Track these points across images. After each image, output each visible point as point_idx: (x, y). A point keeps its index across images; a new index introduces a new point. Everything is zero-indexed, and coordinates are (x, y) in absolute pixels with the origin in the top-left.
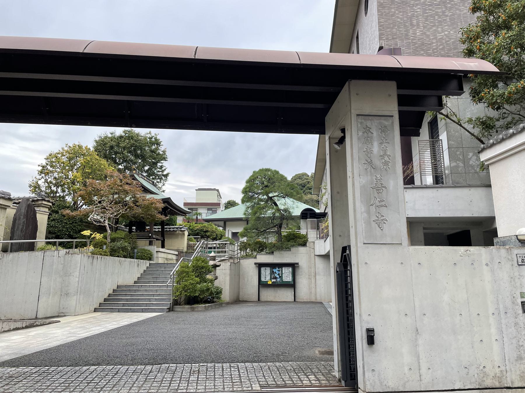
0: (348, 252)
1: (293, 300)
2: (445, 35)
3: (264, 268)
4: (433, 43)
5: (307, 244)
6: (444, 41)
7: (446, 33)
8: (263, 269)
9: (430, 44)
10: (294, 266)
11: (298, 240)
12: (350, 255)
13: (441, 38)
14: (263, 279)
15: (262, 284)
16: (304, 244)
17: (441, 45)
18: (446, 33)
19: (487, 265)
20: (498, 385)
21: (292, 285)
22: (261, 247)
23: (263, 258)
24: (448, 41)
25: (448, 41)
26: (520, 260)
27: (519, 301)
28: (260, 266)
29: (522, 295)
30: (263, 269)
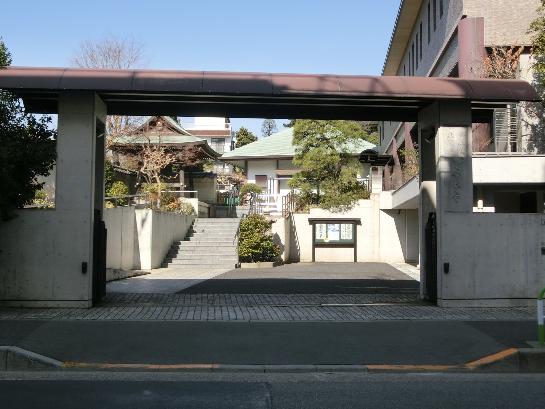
0: (433, 216)
1: (353, 261)
2: (526, 5)
3: (320, 225)
4: (514, 13)
5: (371, 196)
6: (524, 12)
7: (527, 3)
8: (317, 226)
9: (511, 14)
10: (356, 222)
11: (360, 191)
12: (435, 219)
13: (522, 8)
14: (318, 237)
15: (317, 244)
16: (367, 197)
17: (521, 15)
18: (527, 3)
19: (522, 225)
20: (522, 297)
21: (352, 244)
22: (316, 200)
23: (317, 213)
24: (528, 12)
25: (528, 12)
26: (543, 222)
27: (540, 247)
28: (313, 222)
29: (542, 244)
30: (317, 226)
